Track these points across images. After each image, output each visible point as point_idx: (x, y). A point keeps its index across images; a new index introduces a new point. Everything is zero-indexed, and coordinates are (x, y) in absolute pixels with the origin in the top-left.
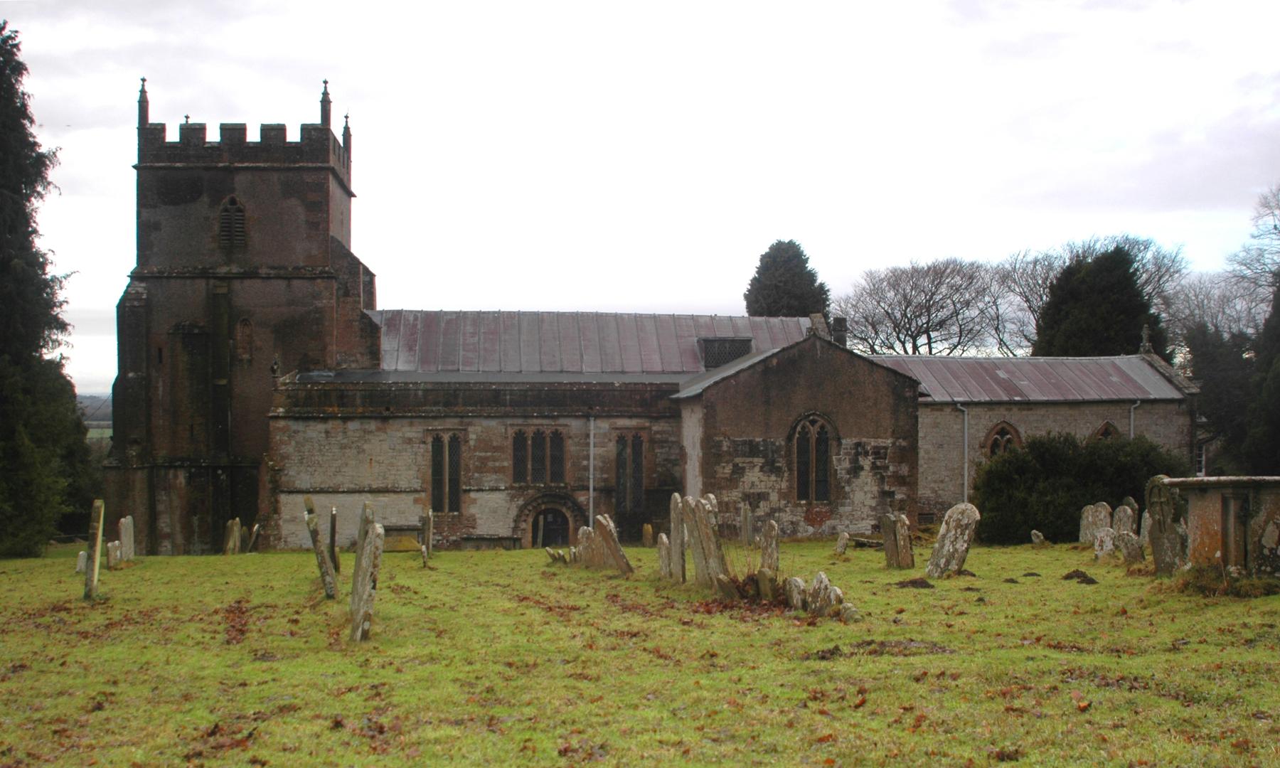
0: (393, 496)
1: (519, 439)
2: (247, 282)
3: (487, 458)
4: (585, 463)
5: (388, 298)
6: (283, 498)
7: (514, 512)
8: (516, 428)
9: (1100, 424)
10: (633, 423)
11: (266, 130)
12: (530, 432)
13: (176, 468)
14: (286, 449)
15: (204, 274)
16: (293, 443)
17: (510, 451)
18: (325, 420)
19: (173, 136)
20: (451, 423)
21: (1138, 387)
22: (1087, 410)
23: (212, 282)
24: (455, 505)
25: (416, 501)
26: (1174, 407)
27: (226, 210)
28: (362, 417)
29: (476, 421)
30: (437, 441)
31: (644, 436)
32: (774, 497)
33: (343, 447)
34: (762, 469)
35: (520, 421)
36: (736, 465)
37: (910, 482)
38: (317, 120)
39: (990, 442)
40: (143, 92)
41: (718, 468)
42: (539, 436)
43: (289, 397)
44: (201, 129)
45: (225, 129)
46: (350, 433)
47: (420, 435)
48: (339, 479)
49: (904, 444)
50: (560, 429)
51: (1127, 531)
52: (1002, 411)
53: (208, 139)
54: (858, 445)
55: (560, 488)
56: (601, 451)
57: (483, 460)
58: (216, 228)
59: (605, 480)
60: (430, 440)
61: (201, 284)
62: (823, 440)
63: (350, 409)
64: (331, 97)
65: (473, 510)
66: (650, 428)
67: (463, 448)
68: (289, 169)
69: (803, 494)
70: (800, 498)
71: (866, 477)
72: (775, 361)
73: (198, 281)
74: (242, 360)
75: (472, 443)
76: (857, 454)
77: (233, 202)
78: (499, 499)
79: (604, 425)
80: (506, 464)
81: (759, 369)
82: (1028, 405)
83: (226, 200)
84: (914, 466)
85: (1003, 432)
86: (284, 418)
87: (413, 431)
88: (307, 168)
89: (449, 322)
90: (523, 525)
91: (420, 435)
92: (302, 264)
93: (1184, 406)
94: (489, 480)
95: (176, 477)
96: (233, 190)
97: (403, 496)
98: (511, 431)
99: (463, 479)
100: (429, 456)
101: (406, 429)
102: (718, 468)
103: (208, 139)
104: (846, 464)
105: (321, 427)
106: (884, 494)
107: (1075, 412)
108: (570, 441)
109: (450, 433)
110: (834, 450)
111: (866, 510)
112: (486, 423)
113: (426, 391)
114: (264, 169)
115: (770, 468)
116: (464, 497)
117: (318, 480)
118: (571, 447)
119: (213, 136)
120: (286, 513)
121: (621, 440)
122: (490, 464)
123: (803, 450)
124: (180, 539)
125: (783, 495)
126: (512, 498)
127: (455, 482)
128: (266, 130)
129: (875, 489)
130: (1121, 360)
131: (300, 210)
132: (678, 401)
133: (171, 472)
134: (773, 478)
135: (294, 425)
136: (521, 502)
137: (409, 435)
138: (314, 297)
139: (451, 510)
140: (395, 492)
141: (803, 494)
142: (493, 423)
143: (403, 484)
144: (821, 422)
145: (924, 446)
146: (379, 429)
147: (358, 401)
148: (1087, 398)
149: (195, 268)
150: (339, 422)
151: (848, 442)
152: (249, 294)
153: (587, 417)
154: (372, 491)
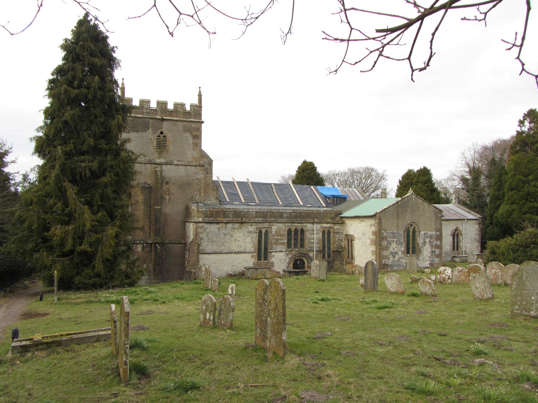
0: (244, 255)
1: (289, 231)
2: (168, 166)
4: (312, 241)
6: (201, 256)
7: (288, 260)
8: (289, 227)
10: (328, 225)
12: (293, 229)
13: (137, 244)
15: (150, 163)
16: (205, 233)
18: (218, 223)
22: (451, 222)
23: (153, 165)
24: (266, 258)
25: (252, 256)
26: (474, 221)
27: (159, 136)
28: (232, 222)
29: (274, 224)
30: (260, 232)
31: (332, 231)
32: (400, 253)
33: (225, 235)
35: (290, 224)
36: (388, 241)
38: (196, 102)
41: (382, 243)
42: (296, 230)
43: (203, 214)
45: (158, 103)
46: (228, 229)
47: (255, 230)
48: (223, 248)
50: (304, 228)
54: (425, 234)
55: (303, 250)
58: (155, 144)
59: (319, 247)
62: (414, 232)
63: (226, 219)
64: (202, 94)
65: (273, 260)
67: (270, 235)
68: (186, 121)
69: (408, 253)
71: (427, 245)
73: (148, 165)
75: (273, 233)
77: (162, 133)
79: (319, 226)
80: (285, 241)
81: (396, 205)
83: (159, 132)
84: (441, 242)
85: (456, 230)
86: (202, 222)
87: (252, 228)
91: (255, 230)
92: (190, 160)
94: (279, 248)
95: (136, 248)
97: (247, 254)
98: (287, 229)
101: (250, 227)
102: (382, 243)
104: (422, 241)
105: (217, 226)
106: (432, 252)
108: (307, 233)
109: (265, 229)
111: (428, 257)
112: (278, 225)
113: (256, 212)
114: (177, 121)
115: (399, 243)
116: (269, 254)
117: (214, 248)
118: (307, 235)
119: (153, 105)
121: (324, 232)
122: (280, 241)
123: (408, 236)
125: (403, 253)
126: (287, 255)
127: (266, 249)
128: (176, 105)
131: (190, 138)
133: (134, 245)
134: (400, 246)
135: (206, 226)
136: (290, 256)
137: (250, 230)
138: (196, 174)
139: (264, 260)
140: (244, 253)
142: (281, 225)
143: (248, 250)
145: (444, 235)
147: (231, 216)
150: (224, 224)
151: (422, 233)
154: (235, 253)
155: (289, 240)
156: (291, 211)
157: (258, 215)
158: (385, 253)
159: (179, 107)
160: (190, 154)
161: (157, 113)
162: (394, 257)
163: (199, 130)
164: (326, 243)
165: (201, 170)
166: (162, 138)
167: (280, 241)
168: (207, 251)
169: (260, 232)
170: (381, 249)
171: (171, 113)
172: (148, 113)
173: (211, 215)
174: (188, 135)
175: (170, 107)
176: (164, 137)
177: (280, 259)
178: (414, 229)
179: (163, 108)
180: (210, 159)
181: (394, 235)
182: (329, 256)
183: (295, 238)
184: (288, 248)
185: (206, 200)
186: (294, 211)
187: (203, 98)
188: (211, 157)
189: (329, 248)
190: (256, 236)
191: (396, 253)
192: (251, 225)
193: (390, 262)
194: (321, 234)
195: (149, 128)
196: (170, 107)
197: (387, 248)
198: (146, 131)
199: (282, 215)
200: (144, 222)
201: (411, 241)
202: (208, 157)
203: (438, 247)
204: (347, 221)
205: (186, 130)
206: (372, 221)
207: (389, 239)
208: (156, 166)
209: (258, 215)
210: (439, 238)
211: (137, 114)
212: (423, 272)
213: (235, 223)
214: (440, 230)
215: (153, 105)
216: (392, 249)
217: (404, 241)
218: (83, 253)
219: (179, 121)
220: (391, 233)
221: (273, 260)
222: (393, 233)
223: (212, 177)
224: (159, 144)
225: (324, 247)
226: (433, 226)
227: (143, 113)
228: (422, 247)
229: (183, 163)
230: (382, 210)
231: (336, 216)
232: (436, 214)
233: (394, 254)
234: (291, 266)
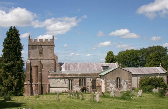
6: (51, 89)
26: (164, 74)
30: (70, 81)
32: (114, 87)
34: (112, 84)
37: (131, 85)
51: (149, 79)
69: (117, 87)
76: (124, 82)
84: (131, 83)
100: (68, 83)
104: (123, 83)
106: (127, 87)
115: (113, 84)
118: (87, 81)
119: (38, 41)
125: (115, 87)
126: (79, 88)
130: (157, 68)
141: (117, 87)
148: (153, 73)
151: (123, 80)
152: (43, 62)
174: (49, 49)
177: (77, 89)
178: (120, 79)
181: (111, 82)
183: (82, 81)
189: (95, 86)
191: (113, 87)
193: (110, 91)
195: (37, 48)
197: (109, 86)
203: (129, 85)
212: (150, 91)
224: (40, 53)
225: (93, 85)
226: (128, 78)
227: (35, 43)
233: (111, 88)
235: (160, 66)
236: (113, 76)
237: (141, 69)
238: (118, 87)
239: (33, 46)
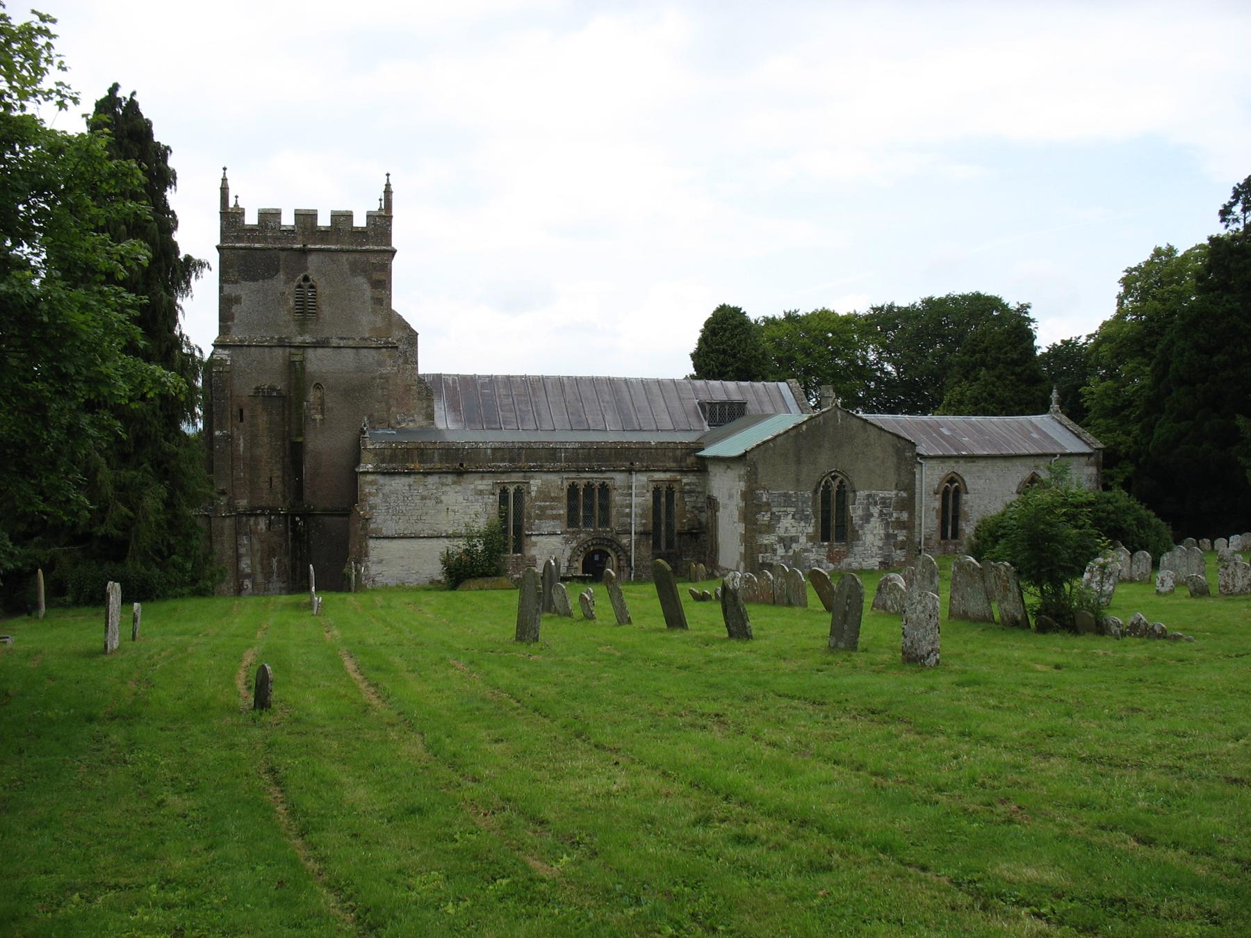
1: (573, 490)
2: (320, 351)
3: (546, 508)
4: (627, 510)
5: (429, 362)
8: (585, 481)
9: (1027, 474)
10: (667, 476)
11: (336, 216)
12: (581, 484)
13: (257, 515)
14: (372, 500)
15: (281, 344)
17: (565, 501)
19: (251, 219)
20: (516, 477)
21: (1060, 446)
22: (1018, 462)
23: (288, 350)
26: (1083, 460)
27: (299, 286)
28: (441, 473)
29: (536, 475)
30: (504, 492)
31: (676, 487)
32: (803, 540)
33: (423, 498)
34: (793, 517)
35: (573, 475)
36: (773, 514)
39: (942, 489)
40: (224, 180)
42: (589, 487)
44: (277, 214)
45: (299, 215)
46: (430, 486)
48: (419, 526)
49: (905, 495)
52: (952, 463)
53: (355, 225)
54: (869, 496)
56: (640, 500)
57: (542, 509)
58: (292, 303)
59: (644, 525)
60: (498, 491)
61: (279, 352)
62: (842, 492)
63: (429, 465)
64: (393, 188)
65: (533, 552)
66: (680, 481)
67: (526, 498)
69: (825, 537)
70: (823, 540)
72: (804, 427)
74: (315, 420)
75: (533, 494)
77: (306, 279)
78: (556, 541)
79: (642, 478)
80: (561, 512)
81: (792, 433)
82: (972, 458)
85: (952, 481)
87: (485, 484)
88: (364, 248)
89: (483, 386)
90: (576, 565)
92: (367, 336)
93: (1092, 459)
94: (547, 526)
95: (256, 524)
96: (306, 269)
98: (566, 484)
99: (526, 525)
103: (355, 225)
104: (860, 512)
106: (888, 536)
107: (1008, 464)
108: (615, 492)
110: (850, 501)
111: (875, 550)
112: (545, 476)
113: (494, 450)
114: (336, 251)
115: (800, 517)
116: (526, 541)
118: (616, 498)
119: (288, 220)
120: (373, 555)
121: (656, 493)
122: (549, 512)
124: (260, 578)
125: (811, 538)
126: (567, 541)
127: (518, 529)
128: (336, 216)
129: (882, 532)
130: (1035, 419)
131: (367, 287)
132: (703, 458)
134: (803, 524)
135: (381, 480)
136: (574, 544)
137: (480, 487)
144: (840, 477)
146: (454, 483)
147: (436, 458)
148: (1018, 452)
149: (272, 338)
151: (861, 494)
152: (316, 361)
153: (630, 471)
154: (447, 537)
155: (572, 510)
156: (577, 446)
157: (499, 454)
158: (767, 539)
159: (342, 219)
160: (367, 323)
161: (295, 238)
162: (787, 548)
163: (386, 269)
164: (663, 516)
165: (390, 356)
166: (306, 289)
167: (549, 512)
168: (385, 533)
169: (504, 492)
170: (754, 530)
171: (325, 234)
172: (276, 239)
173: (393, 458)
174: (361, 280)
175: (324, 221)
176: (312, 287)
179: (308, 225)
180: (412, 331)
181: (787, 500)
182: (670, 544)
183: (588, 505)
184: (569, 526)
185: (404, 420)
186: (584, 446)
187: (395, 197)
188: (413, 326)
189: (669, 526)
190: (493, 500)
191: (794, 539)
192: (482, 478)
194: (649, 496)
196: (324, 221)
198: (271, 277)
199: (554, 454)
200: (271, 470)
201: (833, 513)
202: (406, 326)
203: (900, 524)
204: (712, 469)
205: (355, 269)
206: (742, 470)
207: (774, 510)
208: (293, 350)
209: (499, 454)
210: (908, 504)
211: (253, 241)
213: (447, 473)
214: (910, 488)
215: (288, 220)
216: (782, 530)
217: (815, 513)
218: (105, 538)
219: (342, 251)
220: (780, 495)
221: (533, 552)
222: (785, 495)
223: (417, 369)
225: (656, 524)
227: (265, 239)
228: (862, 527)
229: (351, 343)
230: (758, 446)
231: (689, 455)
232: (899, 452)
233: (787, 542)
234: (578, 565)
235: (1055, 406)
236: (798, 462)
237: (945, 425)
238: (828, 540)
239: (258, 250)
